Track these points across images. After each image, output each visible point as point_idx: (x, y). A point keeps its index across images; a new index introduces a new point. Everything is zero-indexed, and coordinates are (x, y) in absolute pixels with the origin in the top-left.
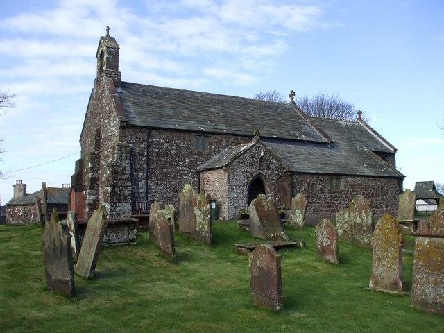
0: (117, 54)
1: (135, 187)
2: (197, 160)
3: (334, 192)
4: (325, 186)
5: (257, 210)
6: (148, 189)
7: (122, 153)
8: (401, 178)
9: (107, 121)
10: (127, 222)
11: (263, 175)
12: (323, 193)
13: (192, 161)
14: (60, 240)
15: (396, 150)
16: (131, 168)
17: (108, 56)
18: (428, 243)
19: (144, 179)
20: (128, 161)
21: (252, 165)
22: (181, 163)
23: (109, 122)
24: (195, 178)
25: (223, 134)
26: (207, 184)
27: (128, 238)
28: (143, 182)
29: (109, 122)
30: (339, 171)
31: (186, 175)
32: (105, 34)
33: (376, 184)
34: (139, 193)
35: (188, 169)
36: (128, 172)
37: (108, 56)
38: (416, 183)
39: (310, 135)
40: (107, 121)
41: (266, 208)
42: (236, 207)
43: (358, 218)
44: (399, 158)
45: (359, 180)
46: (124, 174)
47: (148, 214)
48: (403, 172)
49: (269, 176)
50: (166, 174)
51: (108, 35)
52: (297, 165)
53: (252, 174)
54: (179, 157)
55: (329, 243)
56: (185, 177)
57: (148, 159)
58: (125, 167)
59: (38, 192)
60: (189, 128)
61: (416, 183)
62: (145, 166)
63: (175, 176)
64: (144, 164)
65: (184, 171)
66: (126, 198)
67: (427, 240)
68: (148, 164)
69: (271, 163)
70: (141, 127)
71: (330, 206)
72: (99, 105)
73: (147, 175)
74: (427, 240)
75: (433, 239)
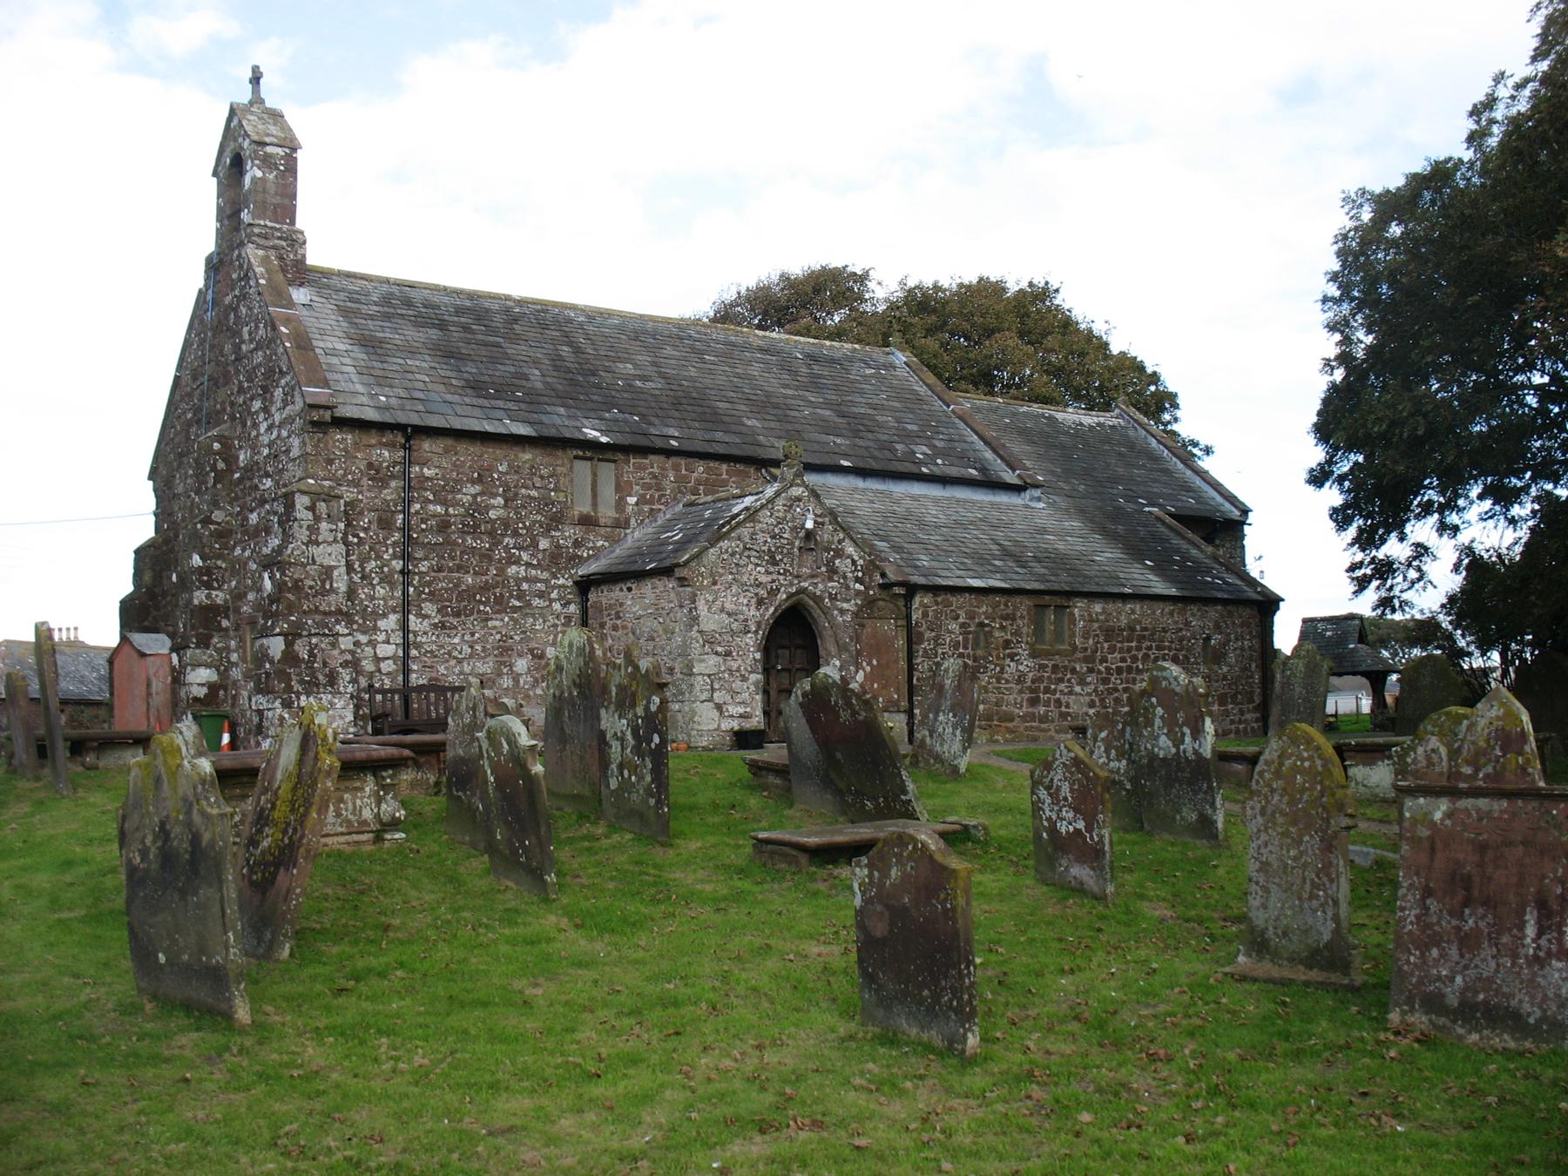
0: (290, 168)
1: (363, 639)
2: (577, 544)
3: (1048, 654)
4: (1017, 633)
5: (812, 722)
6: (406, 646)
7: (317, 519)
8: (1268, 604)
9: (257, 405)
10: (361, 762)
11: (814, 597)
12: (1012, 657)
13: (558, 546)
14: (189, 824)
15: (1245, 512)
16: (350, 567)
17: (254, 173)
18: (1449, 815)
19: (395, 612)
20: (341, 548)
21: (775, 563)
22: (525, 556)
23: (266, 410)
24: (572, 608)
25: (669, 453)
26: (615, 628)
27: (377, 816)
28: (391, 622)
29: (266, 410)
30: (1062, 582)
31: (541, 595)
32: (244, 95)
33: (1187, 624)
34: (377, 660)
35: (545, 575)
36: (341, 586)
37: (254, 173)
38: (1305, 621)
39: (964, 458)
40: (257, 405)
41: (845, 716)
42: (719, 707)
43: (1163, 739)
44: (1255, 541)
45: (1125, 614)
46: (324, 593)
47: (441, 726)
48: (1272, 583)
49: (833, 598)
50: (469, 594)
51: (257, 99)
52: (924, 561)
53: (773, 593)
54: (516, 534)
55: (1081, 825)
56: (536, 602)
57: (408, 541)
58: (330, 569)
59: (76, 646)
60: (553, 432)
61: (1305, 621)
62: (398, 565)
63: (499, 600)
64: (394, 557)
65: (536, 580)
66: (332, 679)
67: (1440, 810)
68: (406, 557)
69: (839, 553)
70: (382, 427)
71: (1034, 702)
72: (228, 347)
73: (405, 593)
74: (1444, 808)
75: (1463, 803)
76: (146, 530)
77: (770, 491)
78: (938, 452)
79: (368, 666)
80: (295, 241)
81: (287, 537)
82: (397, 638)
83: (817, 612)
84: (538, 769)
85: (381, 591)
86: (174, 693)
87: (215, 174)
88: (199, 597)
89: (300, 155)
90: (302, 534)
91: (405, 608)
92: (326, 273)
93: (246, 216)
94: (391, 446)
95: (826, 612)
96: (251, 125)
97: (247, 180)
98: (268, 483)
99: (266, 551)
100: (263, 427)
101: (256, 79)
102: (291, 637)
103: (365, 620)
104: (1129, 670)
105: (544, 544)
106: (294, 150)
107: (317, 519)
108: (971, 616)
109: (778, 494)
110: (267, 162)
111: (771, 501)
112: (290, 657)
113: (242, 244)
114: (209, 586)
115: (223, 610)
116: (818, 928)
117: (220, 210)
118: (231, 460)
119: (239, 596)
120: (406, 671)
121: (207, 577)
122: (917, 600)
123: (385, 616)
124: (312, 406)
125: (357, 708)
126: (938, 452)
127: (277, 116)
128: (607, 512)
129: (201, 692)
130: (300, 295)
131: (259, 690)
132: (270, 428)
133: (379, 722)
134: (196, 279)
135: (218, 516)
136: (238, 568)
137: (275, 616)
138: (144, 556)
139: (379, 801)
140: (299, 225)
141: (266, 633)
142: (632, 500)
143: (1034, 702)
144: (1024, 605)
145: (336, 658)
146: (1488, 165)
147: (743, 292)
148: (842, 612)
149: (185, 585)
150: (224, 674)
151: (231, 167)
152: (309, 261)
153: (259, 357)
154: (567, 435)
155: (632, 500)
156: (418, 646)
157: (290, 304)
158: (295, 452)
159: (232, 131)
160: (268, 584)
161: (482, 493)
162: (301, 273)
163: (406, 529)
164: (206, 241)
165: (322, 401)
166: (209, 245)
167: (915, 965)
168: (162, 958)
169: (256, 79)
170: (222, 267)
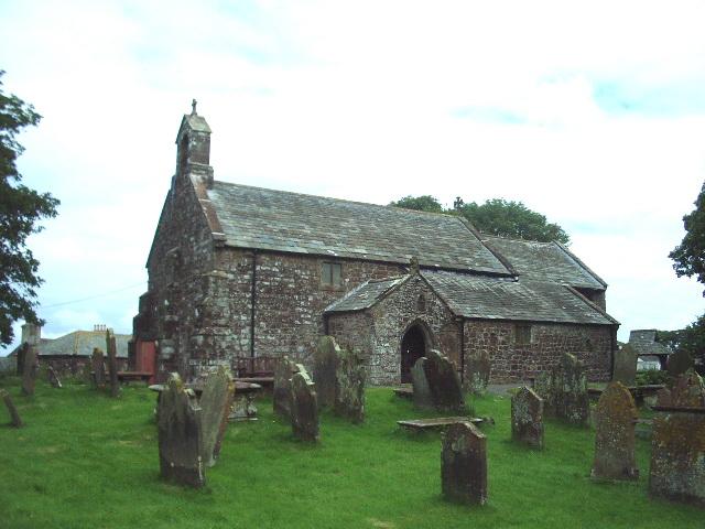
0: (208, 141)
1: (235, 337)
2: (324, 299)
5: (428, 374)
6: (252, 339)
8: (615, 326)
15: (606, 286)
17: (192, 145)
32: (189, 112)
34: (241, 346)
37: (192, 145)
38: (632, 332)
39: (485, 263)
51: (194, 113)
61: (632, 332)
62: (250, 306)
68: (253, 303)
69: (434, 304)
76: (144, 289)
77: (406, 278)
78: (477, 260)
79: (237, 348)
80: (209, 171)
81: (206, 294)
82: (249, 336)
83: (424, 328)
84: (314, 393)
85: (243, 318)
86: (156, 357)
87: (177, 142)
88: (168, 317)
89: (211, 135)
90: (211, 292)
91: (252, 324)
92: (220, 183)
93: (189, 161)
94: (248, 256)
95: (428, 329)
96: (194, 125)
97: (190, 145)
98: (197, 271)
99: (196, 299)
100: (195, 249)
101: (194, 105)
102: (206, 336)
103: (237, 328)
104: (555, 354)
105: (310, 299)
106: (209, 133)
107: (217, 287)
108: (488, 330)
109: (408, 279)
110: (199, 139)
111: (406, 282)
112: (206, 344)
113: (188, 172)
114: (171, 313)
115: (176, 324)
116: (427, 462)
117: (178, 157)
118: (181, 262)
119: (183, 318)
120: (253, 351)
121: (171, 310)
122: (466, 324)
123: (244, 327)
124: (214, 240)
125: (232, 366)
126: (477, 260)
127: (202, 120)
128: (337, 286)
129: (168, 357)
130: (212, 194)
131: (192, 358)
132: (198, 249)
133: (241, 372)
134: (168, 186)
135: (176, 284)
136: (183, 306)
137: (200, 327)
138: (143, 299)
139: (248, 405)
140: (211, 164)
141: (196, 334)
142: (347, 280)
143: (514, 367)
144: (512, 331)
145: (224, 345)
146: (482, 208)
147: (34, 308)
148: (435, 328)
149: (161, 312)
150: (177, 351)
151: (184, 140)
152: (215, 179)
153: (194, 219)
154: (323, 253)
155: (347, 280)
156: (258, 340)
157: (207, 197)
158: (209, 259)
159: (184, 125)
160: (197, 314)
161: (286, 277)
162: (210, 183)
163: (253, 292)
164: (172, 170)
165: (220, 238)
166: (173, 172)
167: (464, 477)
168: (172, 464)
169: (194, 105)
170: (180, 181)
